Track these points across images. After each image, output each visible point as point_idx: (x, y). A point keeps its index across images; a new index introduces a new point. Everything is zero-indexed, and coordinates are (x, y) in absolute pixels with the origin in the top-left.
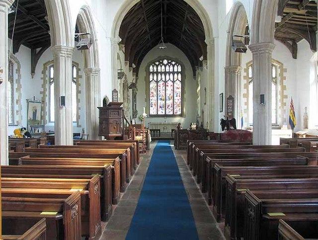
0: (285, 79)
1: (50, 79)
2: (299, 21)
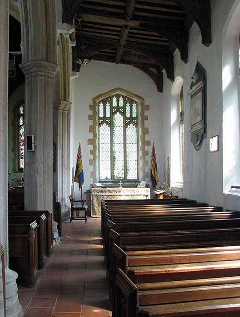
2: (148, 39)
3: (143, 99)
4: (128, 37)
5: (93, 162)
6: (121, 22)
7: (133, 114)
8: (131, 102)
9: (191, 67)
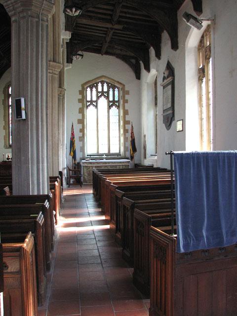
3: (124, 85)
4: (113, 35)
5: (82, 139)
6: (109, 26)
7: (115, 98)
8: (114, 87)
9: (163, 64)
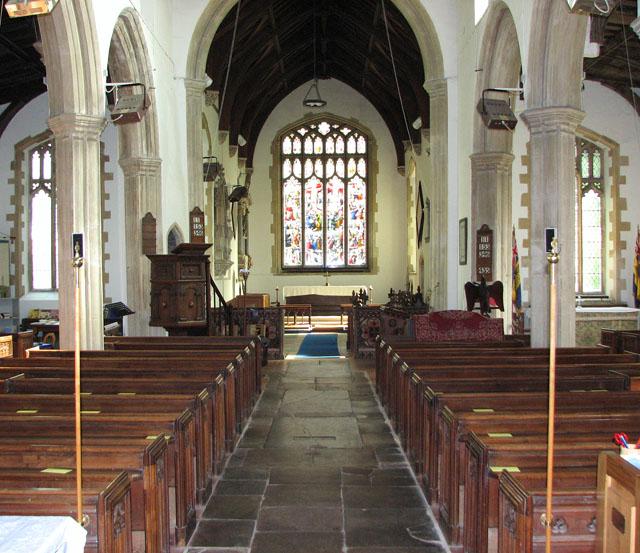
0: (624, 183)
1: (32, 181)
7: (594, 172)
